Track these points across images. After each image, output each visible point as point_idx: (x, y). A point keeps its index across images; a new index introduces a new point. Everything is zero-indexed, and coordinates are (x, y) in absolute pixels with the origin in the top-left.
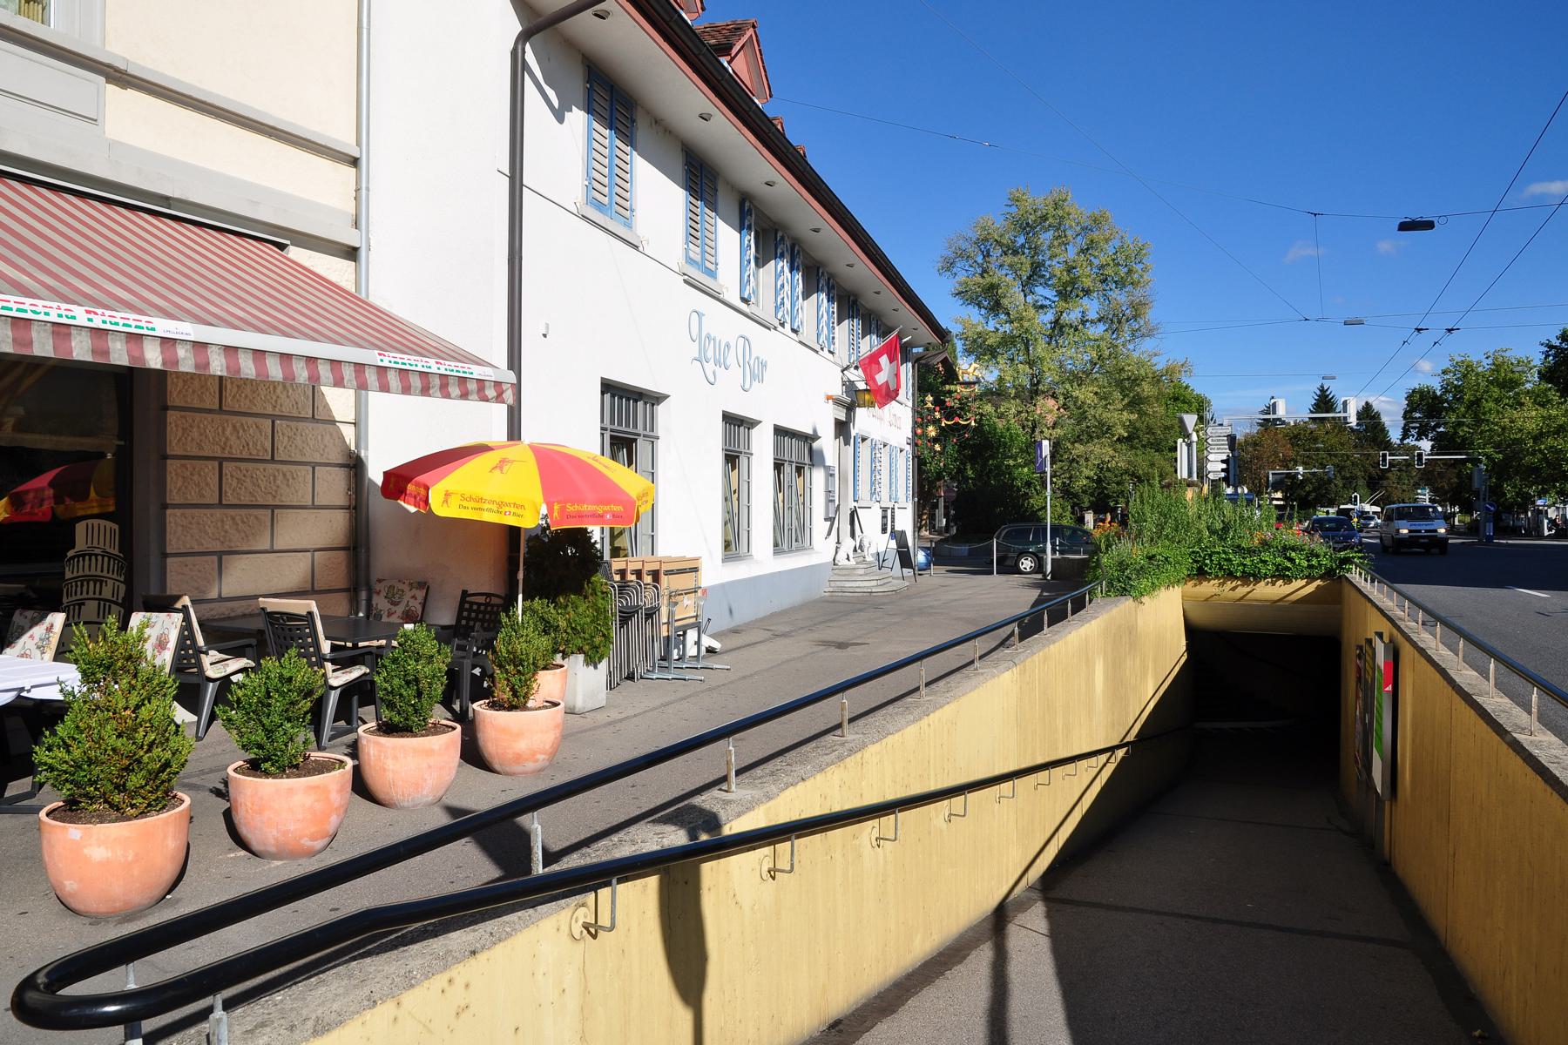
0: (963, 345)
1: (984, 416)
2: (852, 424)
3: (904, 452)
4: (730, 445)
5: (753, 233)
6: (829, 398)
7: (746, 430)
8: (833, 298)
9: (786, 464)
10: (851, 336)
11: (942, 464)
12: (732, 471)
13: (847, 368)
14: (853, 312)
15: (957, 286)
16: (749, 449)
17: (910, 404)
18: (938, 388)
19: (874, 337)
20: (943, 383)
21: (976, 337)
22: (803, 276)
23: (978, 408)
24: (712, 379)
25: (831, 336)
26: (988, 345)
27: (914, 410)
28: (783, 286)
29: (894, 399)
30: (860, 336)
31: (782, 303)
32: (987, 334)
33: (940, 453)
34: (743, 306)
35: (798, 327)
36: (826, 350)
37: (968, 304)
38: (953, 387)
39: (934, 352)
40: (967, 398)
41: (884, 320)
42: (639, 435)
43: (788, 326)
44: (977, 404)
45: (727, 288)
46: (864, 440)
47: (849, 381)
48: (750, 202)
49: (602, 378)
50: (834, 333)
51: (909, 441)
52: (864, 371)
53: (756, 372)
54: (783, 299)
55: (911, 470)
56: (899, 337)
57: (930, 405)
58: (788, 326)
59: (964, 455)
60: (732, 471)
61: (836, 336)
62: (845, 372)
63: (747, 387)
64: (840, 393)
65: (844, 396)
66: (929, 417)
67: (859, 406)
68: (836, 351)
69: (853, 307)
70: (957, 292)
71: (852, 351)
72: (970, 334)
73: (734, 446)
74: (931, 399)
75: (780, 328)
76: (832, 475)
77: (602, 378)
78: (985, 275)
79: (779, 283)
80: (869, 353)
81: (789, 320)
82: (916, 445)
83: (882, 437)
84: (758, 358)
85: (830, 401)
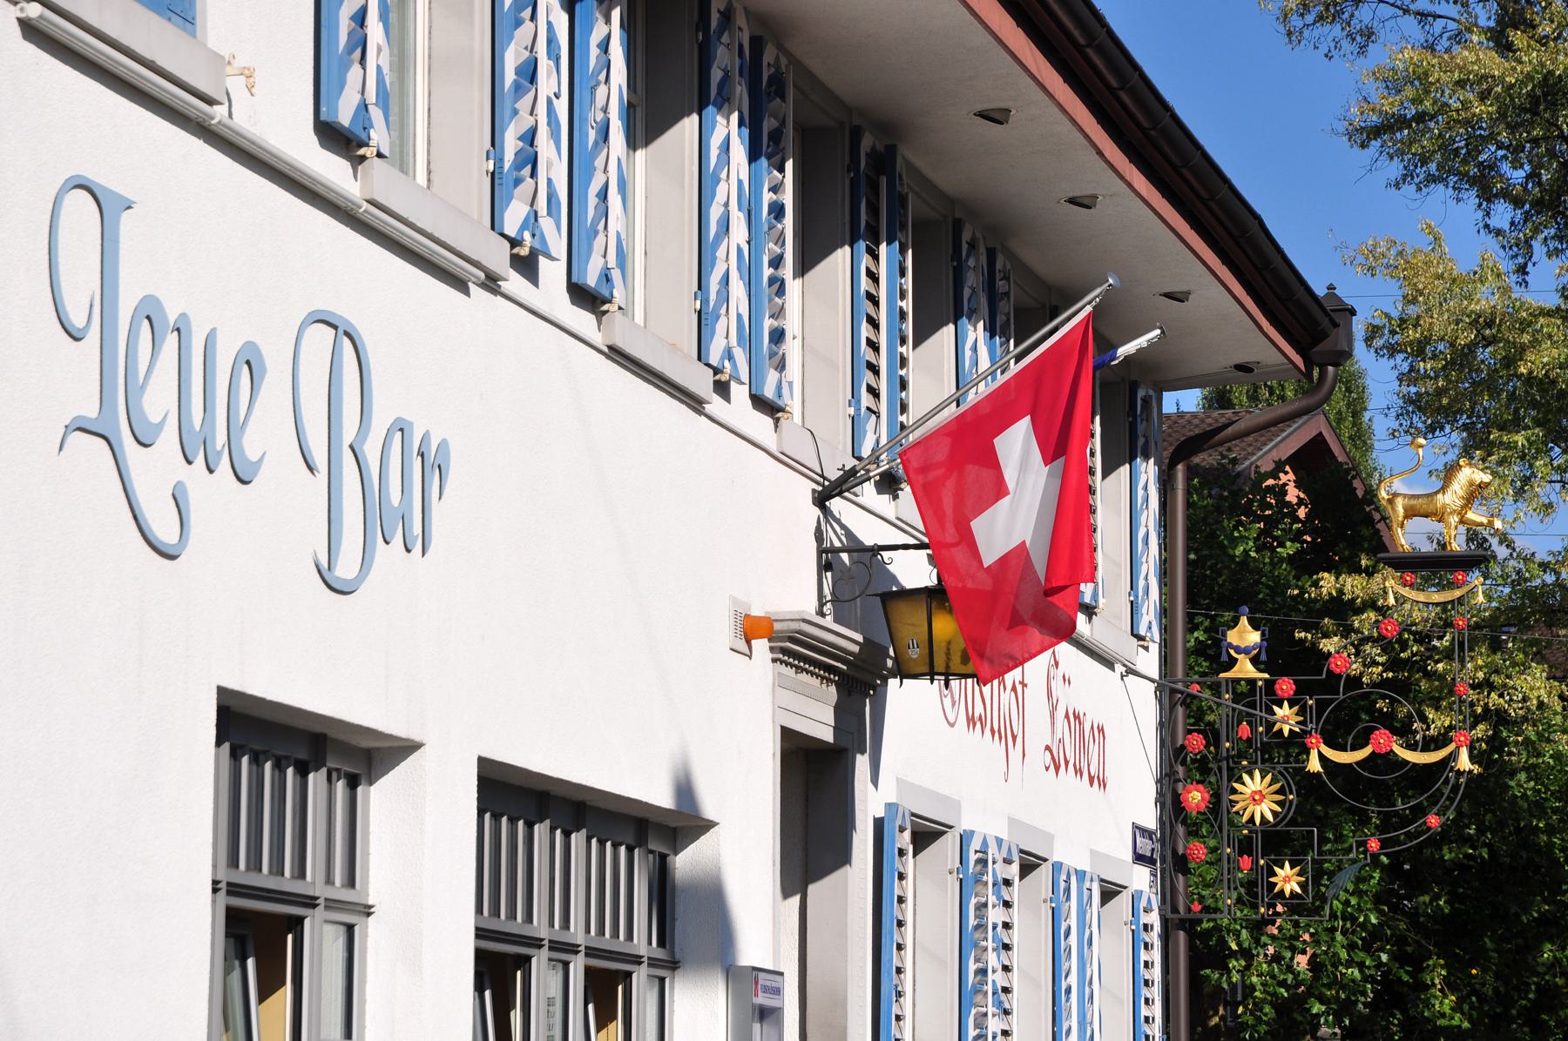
0: (1404, 378)
1: (1514, 724)
2: (862, 763)
3: (1122, 902)
4: (255, 864)
5: (789, 165)
6: (751, 629)
7: (340, 786)
8: (776, 136)
9: (540, 962)
10: (865, 330)
11: (1302, 962)
12: (262, 998)
13: (843, 484)
14: (874, 210)
15: (1375, 91)
16: (351, 882)
17: (1149, 662)
18: (1278, 588)
19: (976, 333)
20: (1308, 564)
21: (1466, 337)
22: (628, 26)
23: (1487, 685)
24: (165, 529)
25: (768, 323)
26: (1529, 379)
27: (1169, 694)
28: (529, 73)
29: (1066, 632)
30: (909, 328)
31: (529, 160)
32: (1525, 325)
33: (1296, 905)
34: (330, 169)
35: (606, 277)
36: (740, 393)
37: (1431, 179)
38: (1353, 585)
39: (1260, 414)
40: (1422, 638)
41: (1029, 256)
42: (310, 902)
43: (553, 273)
44: (1476, 665)
45: (248, 74)
46: (925, 835)
47: (855, 547)
48: (781, 47)
49: (482, 761)
50: (779, 313)
51: (1145, 846)
52: (925, 501)
53: (395, 496)
54: (530, 137)
55: (1156, 993)
56: (1101, 333)
57: (1245, 669)
58: (553, 273)
59: (1413, 916)
60: (262, 998)
61: (792, 324)
62: (836, 504)
63: (346, 568)
64: (809, 606)
65: (828, 621)
66: (1244, 730)
67: (904, 673)
68: (794, 404)
69: (875, 188)
70: (1374, 119)
71: (866, 399)
72: (1439, 323)
73: (278, 869)
74: (1254, 637)
75: (514, 283)
76: (768, 1015)
77: (482, 761)
78: (1518, 38)
79: (512, 59)
80: (951, 411)
81: (558, 246)
82: (1181, 864)
83: (1013, 822)
84: (402, 428)
85: (761, 646)
